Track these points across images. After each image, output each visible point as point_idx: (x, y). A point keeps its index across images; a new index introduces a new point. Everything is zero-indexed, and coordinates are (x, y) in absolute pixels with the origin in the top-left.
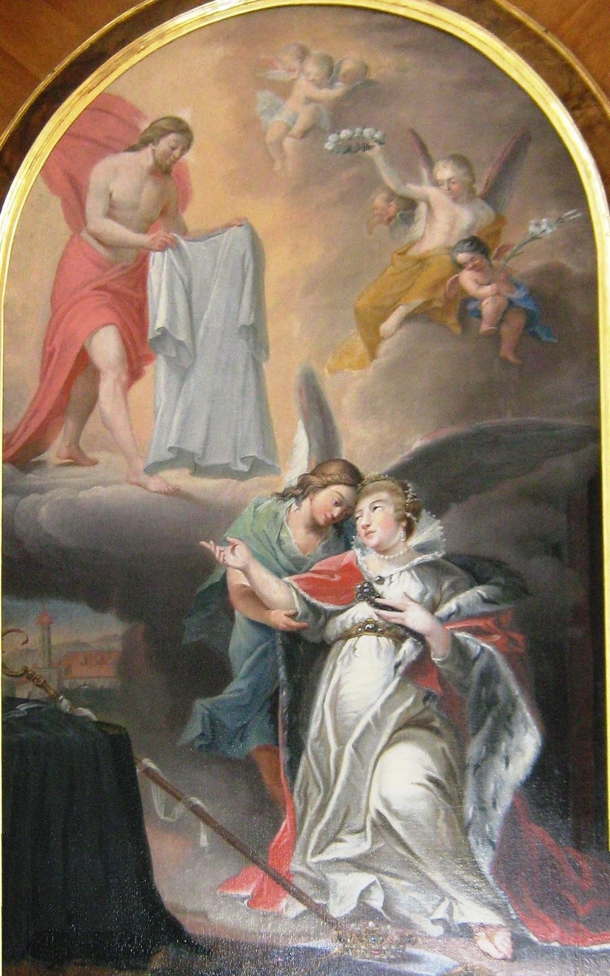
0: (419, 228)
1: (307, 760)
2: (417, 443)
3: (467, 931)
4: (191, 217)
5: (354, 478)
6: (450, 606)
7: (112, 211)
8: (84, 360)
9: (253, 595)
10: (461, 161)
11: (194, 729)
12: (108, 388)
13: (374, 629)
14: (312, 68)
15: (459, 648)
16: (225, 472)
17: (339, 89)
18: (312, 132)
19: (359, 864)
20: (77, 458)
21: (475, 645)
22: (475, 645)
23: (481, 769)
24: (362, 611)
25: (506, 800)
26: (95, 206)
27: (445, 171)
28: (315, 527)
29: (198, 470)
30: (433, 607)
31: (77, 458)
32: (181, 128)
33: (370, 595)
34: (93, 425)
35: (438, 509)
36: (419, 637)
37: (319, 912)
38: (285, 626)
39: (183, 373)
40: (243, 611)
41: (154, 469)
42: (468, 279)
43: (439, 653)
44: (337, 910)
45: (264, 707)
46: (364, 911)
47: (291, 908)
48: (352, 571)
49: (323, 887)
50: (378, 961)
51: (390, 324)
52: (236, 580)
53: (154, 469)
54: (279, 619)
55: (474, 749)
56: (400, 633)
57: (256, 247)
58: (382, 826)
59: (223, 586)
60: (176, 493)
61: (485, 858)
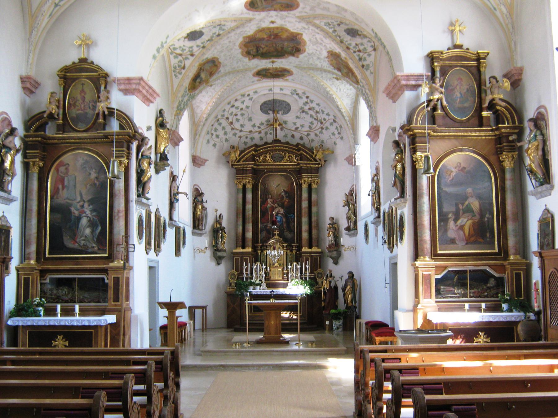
0: (91, 176)
1: (79, 229)
2: (90, 198)
3: (93, 247)
4: (69, 174)
5: (84, 201)
6: (93, 214)
7: (61, 173)
8: (58, 188)
9: (74, 213)
10: (95, 169)
11: (68, 226)
12: (60, 191)
13: (86, 216)
14: (81, 159)
15: (93, 219)
16: (72, 200)
17: (84, 161)
18: (82, 166)
19: (84, 240)
20: (57, 198)
21: (95, 218)
22: (95, 218)
23: (95, 231)
24: (84, 215)
25: (98, 234)
26: (60, 172)
27: (94, 170)
28: (80, 206)
29: (69, 200)
30: (91, 214)
31: (57, 198)
32: (69, 165)
33: (85, 213)
34: (59, 195)
35: (92, 205)
36: (90, 217)
37: (79, 245)
38: (146, 179)
39: (68, 190)
40: (73, 214)
41: (65, 200)
42: (96, 182)
43: (92, 219)
44: (81, 245)
45: (259, 49)
46: (84, 245)
47: (77, 244)
48: (84, 211)
49: (80, 242)
50: (103, 139)
51: (88, 186)
52: (72, 211)
53: (65, 200)
54: (76, 215)
55: (95, 229)
56: (88, 217)
57: (75, 177)
58: (86, 237)
59: (71, 212)
60: (67, 202)
61: (95, 240)
